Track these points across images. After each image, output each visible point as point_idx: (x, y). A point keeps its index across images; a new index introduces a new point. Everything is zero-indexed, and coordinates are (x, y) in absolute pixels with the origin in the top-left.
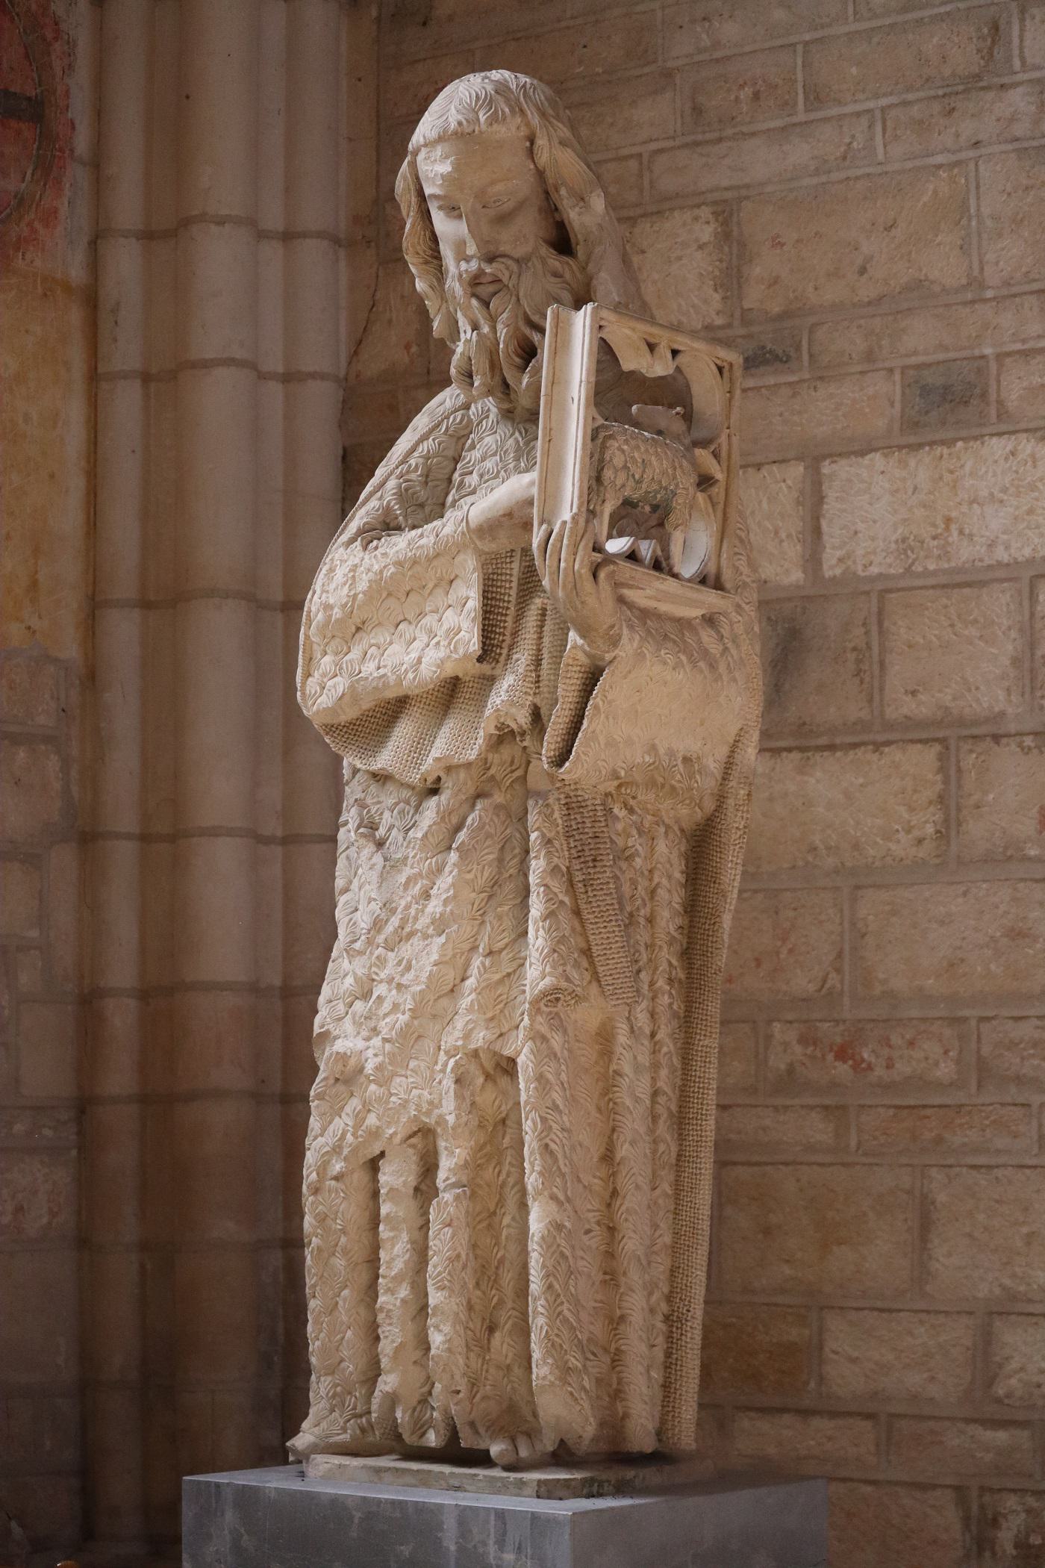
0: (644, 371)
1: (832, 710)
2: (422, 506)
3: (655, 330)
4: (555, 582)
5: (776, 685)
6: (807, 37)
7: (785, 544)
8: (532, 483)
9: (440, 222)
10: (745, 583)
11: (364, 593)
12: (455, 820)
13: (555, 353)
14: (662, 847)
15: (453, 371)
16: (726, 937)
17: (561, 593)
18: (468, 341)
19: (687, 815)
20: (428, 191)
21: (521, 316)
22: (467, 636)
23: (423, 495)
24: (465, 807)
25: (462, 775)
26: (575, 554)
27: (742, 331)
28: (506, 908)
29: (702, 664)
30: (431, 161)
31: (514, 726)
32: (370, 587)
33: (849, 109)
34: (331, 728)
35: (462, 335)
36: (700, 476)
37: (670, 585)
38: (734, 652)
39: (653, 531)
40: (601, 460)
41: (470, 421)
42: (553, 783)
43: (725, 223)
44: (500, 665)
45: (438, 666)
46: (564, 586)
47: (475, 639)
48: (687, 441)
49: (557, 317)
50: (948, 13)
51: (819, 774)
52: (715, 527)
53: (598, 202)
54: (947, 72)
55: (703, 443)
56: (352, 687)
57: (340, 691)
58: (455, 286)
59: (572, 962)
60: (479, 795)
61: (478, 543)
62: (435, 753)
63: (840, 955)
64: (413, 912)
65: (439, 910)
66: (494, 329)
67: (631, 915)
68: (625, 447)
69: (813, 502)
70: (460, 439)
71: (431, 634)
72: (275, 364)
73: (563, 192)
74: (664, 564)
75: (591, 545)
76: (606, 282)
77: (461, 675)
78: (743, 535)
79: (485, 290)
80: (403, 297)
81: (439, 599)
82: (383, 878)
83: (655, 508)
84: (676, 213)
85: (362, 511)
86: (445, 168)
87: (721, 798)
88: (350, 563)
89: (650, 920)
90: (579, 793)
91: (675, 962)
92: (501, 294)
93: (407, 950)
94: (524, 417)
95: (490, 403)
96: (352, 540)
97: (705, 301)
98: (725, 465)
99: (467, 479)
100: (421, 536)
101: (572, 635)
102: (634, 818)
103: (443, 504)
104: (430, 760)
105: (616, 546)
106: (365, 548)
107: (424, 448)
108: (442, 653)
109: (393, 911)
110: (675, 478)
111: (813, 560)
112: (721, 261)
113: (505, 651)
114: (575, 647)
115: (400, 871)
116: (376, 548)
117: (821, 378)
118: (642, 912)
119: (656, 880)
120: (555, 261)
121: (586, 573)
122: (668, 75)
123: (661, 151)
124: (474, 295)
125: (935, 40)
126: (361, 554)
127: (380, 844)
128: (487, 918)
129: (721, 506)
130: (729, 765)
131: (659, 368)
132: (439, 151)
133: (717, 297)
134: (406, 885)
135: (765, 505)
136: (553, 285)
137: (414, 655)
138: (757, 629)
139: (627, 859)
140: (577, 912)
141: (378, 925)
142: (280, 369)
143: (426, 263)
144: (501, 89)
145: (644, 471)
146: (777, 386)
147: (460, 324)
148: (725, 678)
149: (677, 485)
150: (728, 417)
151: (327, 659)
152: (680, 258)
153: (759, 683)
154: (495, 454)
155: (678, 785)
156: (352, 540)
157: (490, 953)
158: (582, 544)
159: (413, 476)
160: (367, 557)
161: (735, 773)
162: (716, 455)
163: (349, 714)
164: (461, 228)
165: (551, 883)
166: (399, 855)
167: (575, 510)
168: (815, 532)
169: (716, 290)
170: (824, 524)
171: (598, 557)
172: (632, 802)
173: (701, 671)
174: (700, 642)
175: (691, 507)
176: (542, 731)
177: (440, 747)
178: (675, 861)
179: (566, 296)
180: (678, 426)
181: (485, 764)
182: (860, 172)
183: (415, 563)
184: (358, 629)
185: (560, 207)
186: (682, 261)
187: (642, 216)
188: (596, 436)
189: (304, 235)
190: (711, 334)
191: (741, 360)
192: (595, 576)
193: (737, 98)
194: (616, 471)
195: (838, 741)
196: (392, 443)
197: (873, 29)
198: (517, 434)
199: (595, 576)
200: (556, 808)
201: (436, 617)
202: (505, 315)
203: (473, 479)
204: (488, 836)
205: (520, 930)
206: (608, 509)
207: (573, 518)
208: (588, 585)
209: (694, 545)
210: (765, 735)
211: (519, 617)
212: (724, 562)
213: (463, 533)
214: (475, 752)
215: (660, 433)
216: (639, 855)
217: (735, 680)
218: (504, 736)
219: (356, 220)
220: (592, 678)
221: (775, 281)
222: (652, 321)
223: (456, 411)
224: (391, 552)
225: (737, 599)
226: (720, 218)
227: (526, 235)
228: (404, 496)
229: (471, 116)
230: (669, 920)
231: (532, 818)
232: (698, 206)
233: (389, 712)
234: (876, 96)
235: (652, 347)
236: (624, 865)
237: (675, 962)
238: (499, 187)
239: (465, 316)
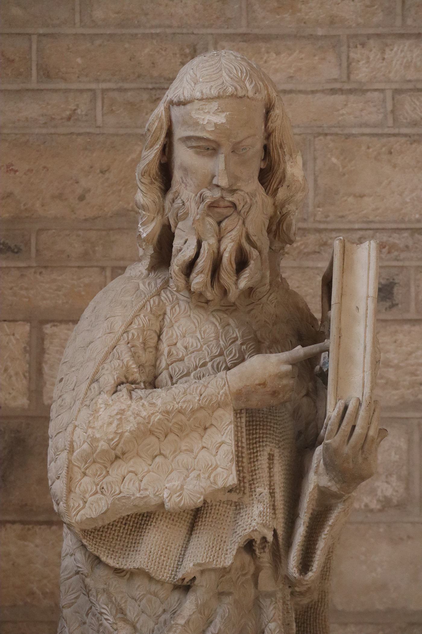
6: (41, 31)
11: (130, 432)
13: (343, 271)
32: (138, 428)
33: (74, 86)
50: (158, 35)
51: (38, 541)
54: (155, 74)
56: (113, 504)
117: (46, 267)
125: (147, 51)
126: (130, 402)
132: (214, 105)
151: (86, 479)
182: (82, 131)
197: (97, 35)
202: (234, 233)
224: (159, 402)
233: (137, 521)
234: (97, 80)
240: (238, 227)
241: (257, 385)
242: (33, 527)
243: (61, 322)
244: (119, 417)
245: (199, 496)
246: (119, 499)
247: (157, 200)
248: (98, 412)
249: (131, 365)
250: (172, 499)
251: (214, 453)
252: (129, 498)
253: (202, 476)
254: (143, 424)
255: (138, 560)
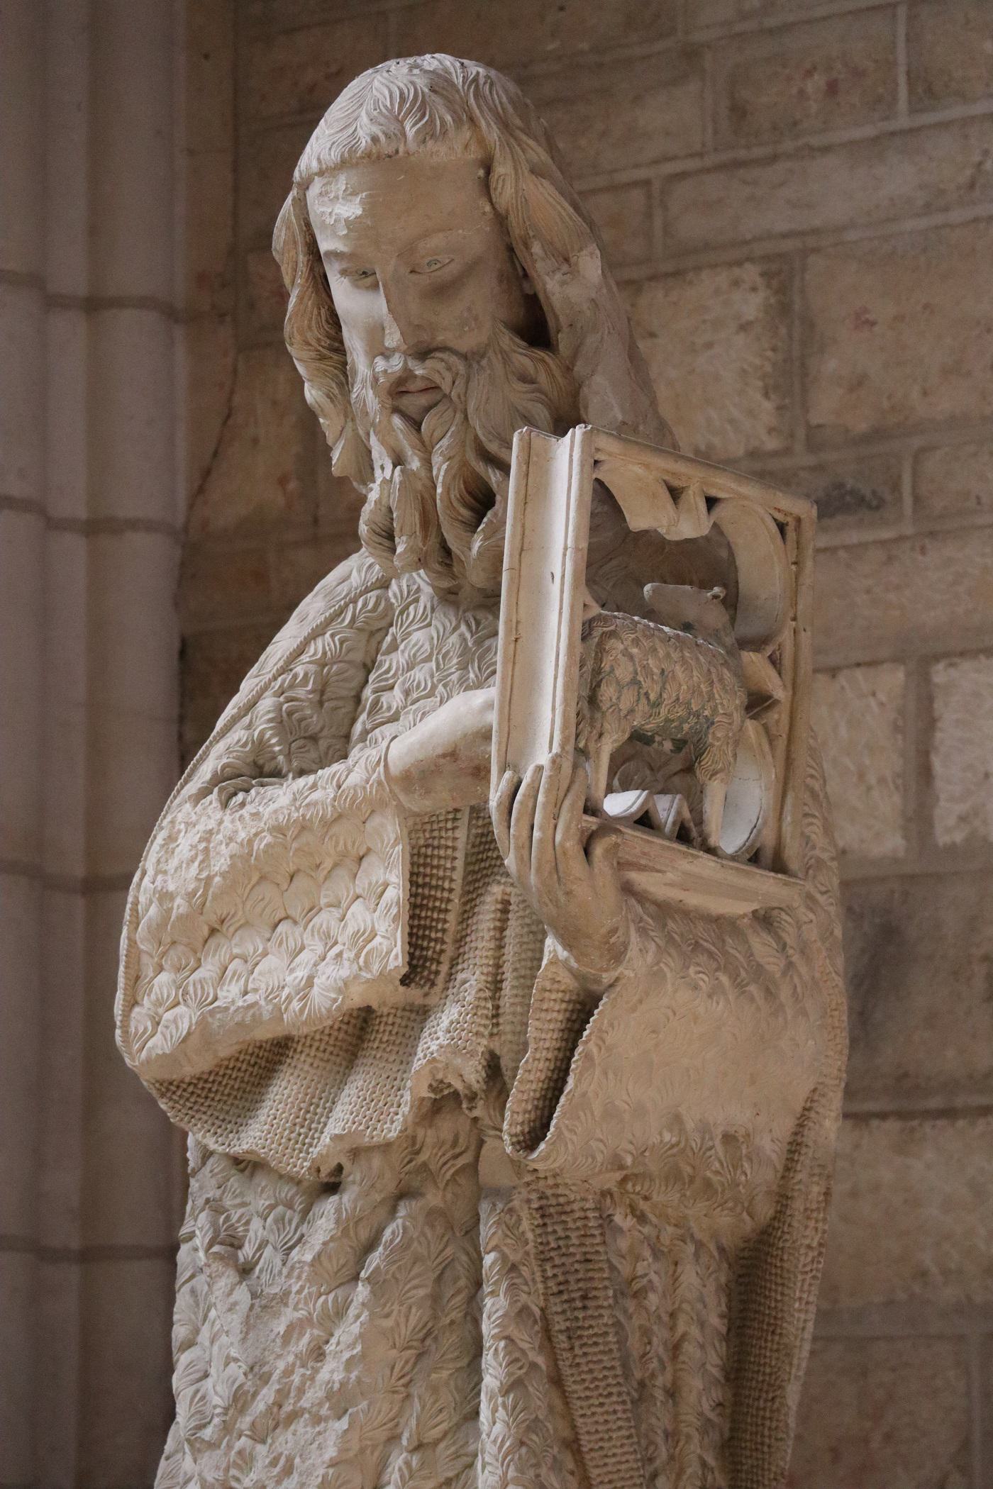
0: (662, 531)
1: (950, 1053)
2: (314, 739)
3: (681, 467)
4: (524, 861)
5: (861, 1014)
7: (875, 794)
8: (489, 706)
9: (344, 294)
10: (819, 861)
12: (364, 1234)
13: (525, 501)
14: (690, 1276)
15: (363, 529)
16: (792, 1422)
17: (533, 879)
18: (388, 482)
19: (727, 1224)
20: (324, 246)
21: (470, 437)
22: (386, 942)
23: (315, 721)
24: (383, 1212)
25: (377, 1161)
26: (556, 817)
27: (810, 460)
28: (445, 1374)
29: (752, 988)
30: (329, 200)
31: (458, 1085)
32: (232, 866)
34: (169, 1087)
35: (378, 472)
36: (750, 694)
37: (705, 865)
38: (803, 969)
39: (676, 780)
40: (597, 671)
41: (390, 606)
42: (519, 1174)
43: (782, 290)
44: (438, 989)
45: (340, 991)
46: (539, 870)
47: (398, 949)
48: (729, 640)
49: (528, 447)
51: (929, 1155)
52: (773, 773)
53: (591, 265)
55: (757, 643)
56: (202, 1022)
57: (184, 1027)
58: (366, 395)
59: (549, 1460)
60: (403, 1194)
61: (402, 797)
62: (335, 1126)
63: (966, 1445)
64: (296, 1379)
65: (338, 1377)
66: (428, 463)
67: (642, 1384)
68: (635, 651)
69: (920, 726)
70: (374, 633)
71: (329, 940)
72: (73, 506)
73: (536, 248)
74: (694, 833)
75: (581, 804)
76: (604, 392)
77: (375, 1006)
78: (817, 786)
79: (413, 403)
80: (275, 403)
81: (340, 886)
82: (249, 1325)
83: (680, 745)
84: (705, 275)
85: (221, 747)
86: (351, 209)
87: (783, 1199)
88: (201, 827)
89: (673, 1393)
90: (560, 1191)
91: (711, 1461)
92: (440, 408)
93: (285, 1441)
94: (475, 600)
95: (422, 579)
96: (205, 792)
97: (751, 413)
98: (788, 676)
99: (385, 698)
100: (314, 787)
101: (550, 942)
102: (646, 1230)
103: (347, 737)
104: (326, 1139)
105: (619, 804)
106: (225, 805)
107: (316, 648)
108: (345, 972)
109: (265, 1379)
110: (711, 697)
111: (919, 818)
112: (774, 350)
113: (444, 968)
114: (554, 962)
115: (277, 1315)
116: (243, 805)
117: (932, 534)
118: (660, 1381)
119: (681, 1328)
120: (524, 358)
121: (573, 846)
122: (691, 54)
123: (683, 175)
124: (396, 410)
126: (219, 815)
127: (245, 1271)
128: (415, 1391)
129: (781, 744)
130: (795, 1147)
131: (687, 525)
132: (342, 182)
133: (768, 406)
134: (287, 1338)
135: (843, 731)
136: (518, 394)
137: (301, 973)
138: (838, 932)
139: (635, 1295)
140: (557, 1381)
141: (240, 1400)
142: (82, 513)
143: (322, 358)
144: (440, 85)
145: (663, 688)
146: (864, 546)
147: (375, 455)
148: (790, 1012)
149: (714, 710)
150: (795, 604)
151: (164, 977)
152: (709, 345)
153: (842, 1018)
154: (428, 659)
155: (715, 1179)
156: (205, 792)
157: (419, 1447)
158: (567, 803)
159: (301, 693)
160: (227, 818)
161: (806, 1158)
162: (775, 661)
163: (200, 1064)
164: (377, 305)
165: (516, 1334)
166: (275, 1290)
167: (556, 749)
168: (922, 774)
169: (766, 395)
170: (937, 763)
171: (592, 822)
172: (643, 1206)
173: (752, 999)
174: (750, 955)
175: (737, 743)
176: (503, 1093)
177: (341, 1119)
178: (711, 1300)
179: (542, 413)
180: (716, 617)
181: (411, 1144)
183: (303, 828)
184: (213, 931)
185: (531, 272)
186: (715, 354)
187: (652, 278)
188: (590, 636)
189: (119, 303)
190: (762, 469)
191: (814, 512)
192: (587, 851)
193: (802, 92)
194: (620, 687)
195: (959, 1102)
196: (264, 640)
198: (463, 628)
199: (587, 851)
200: (524, 1214)
201: (337, 913)
202: (445, 442)
203: (394, 698)
204: (416, 1260)
205: (468, 1409)
206: (607, 747)
207: (553, 761)
208: (576, 864)
209: (740, 804)
210: (849, 1094)
211: (467, 915)
212: (787, 828)
213: (380, 783)
214: (397, 1126)
215: (687, 627)
216: (653, 1289)
217: (804, 1013)
218: (442, 1101)
219: (201, 279)
220: (583, 1008)
221: (858, 383)
222: (673, 451)
223: (367, 590)
224: (267, 812)
225: (809, 886)
226: (775, 283)
227: (478, 316)
228: (285, 722)
229: (393, 128)
230: (701, 1393)
231: (487, 1230)
232: (739, 263)
235: (675, 494)
236: (631, 1305)
237: (711, 1461)
238: (437, 241)
239: (383, 442)
240: (453, 429)
241: (438, 756)
242: (920, 1125)
243: (962, 654)
244: (204, 845)
245: (333, 996)
246: (212, 1013)
247: (336, 392)
248: (176, 840)
249: (269, 739)
250: (291, 1007)
251: (372, 906)
252: (227, 1009)
253: (345, 956)
254: (241, 856)
255: (253, 1137)
